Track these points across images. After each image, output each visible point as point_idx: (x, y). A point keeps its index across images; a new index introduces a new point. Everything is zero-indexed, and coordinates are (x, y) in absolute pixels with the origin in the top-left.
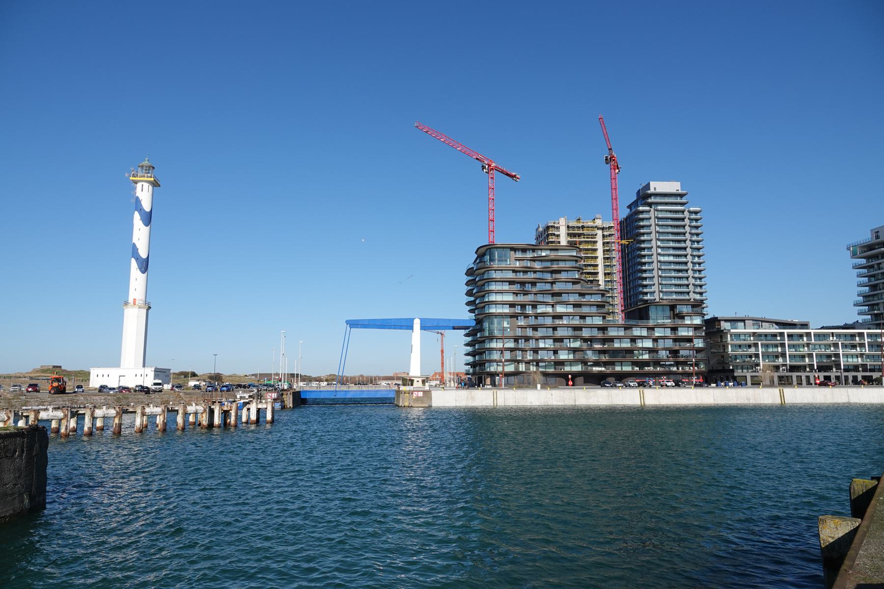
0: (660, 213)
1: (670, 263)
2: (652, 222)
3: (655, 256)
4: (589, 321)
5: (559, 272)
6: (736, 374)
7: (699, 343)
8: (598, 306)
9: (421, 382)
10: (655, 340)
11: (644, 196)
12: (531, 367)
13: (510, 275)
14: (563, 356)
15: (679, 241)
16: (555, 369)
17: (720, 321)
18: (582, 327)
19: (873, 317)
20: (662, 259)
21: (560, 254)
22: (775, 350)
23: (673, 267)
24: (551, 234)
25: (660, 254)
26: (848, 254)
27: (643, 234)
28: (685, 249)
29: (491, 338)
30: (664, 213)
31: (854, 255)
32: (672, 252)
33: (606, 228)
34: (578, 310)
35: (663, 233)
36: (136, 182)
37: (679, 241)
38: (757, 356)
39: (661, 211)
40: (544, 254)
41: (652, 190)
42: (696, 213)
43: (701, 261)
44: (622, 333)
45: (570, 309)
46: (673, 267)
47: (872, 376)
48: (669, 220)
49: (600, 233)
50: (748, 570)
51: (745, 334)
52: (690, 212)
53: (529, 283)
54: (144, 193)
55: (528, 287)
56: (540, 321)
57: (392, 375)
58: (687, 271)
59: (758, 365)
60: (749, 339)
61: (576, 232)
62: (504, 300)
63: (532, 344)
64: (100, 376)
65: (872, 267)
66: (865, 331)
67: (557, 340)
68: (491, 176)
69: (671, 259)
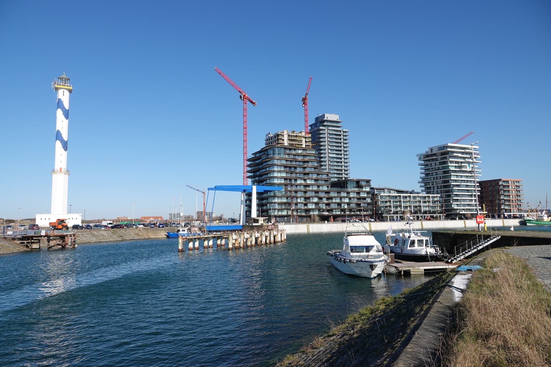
0: (330, 131)
1: (334, 158)
2: (326, 135)
3: (327, 154)
4: (321, 188)
5: (308, 162)
6: (383, 215)
7: (369, 200)
8: (325, 181)
9: (262, 220)
10: (350, 199)
11: (320, 121)
12: (294, 212)
13: (284, 162)
14: (310, 206)
15: (338, 147)
16: (306, 213)
17: (374, 189)
18: (319, 192)
19: (426, 188)
20: (330, 155)
21: (307, 152)
22: (397, 204)
23: (335, 160)
24: (280, 139)
25: (330, 153)
26: (417, 158)
27: (322, 142)
28: (341, 151)
29: (274, 197)
30: (334, 131)
31: (420, 159)
32: (335, 152)
33: (307, 137)
34: (316, 182)
35: (331, 142)
36: (57, 89)
37: (338, 147)
38: (390, 206)
39: (331, 130)
40: (300, 152)
41: (326, 119)
42: (346, 132)
43: (347, 157)
44: (336, 195)
45: (313, 182)
46: (335, 160)
47: (433, 216)
48: (334, 135)
49: (304, 139)
50: (139, 352)
51: (385, 196)
52: (344, 132)
53: (293, 167)
54: (64, 96)
55: (293, 169)
56: (298, 188)
57: (92, 219)
58: (341, 162)
59: (391, 211)
60: (386, 198)
61: (293, 138)
62: (282, 176)
63: (295, 201)
64: (43, 219)
65: (427, 165)
66: (431, 195)
67: (306, 198)
68: (245, 102)
69: (335, 156)
